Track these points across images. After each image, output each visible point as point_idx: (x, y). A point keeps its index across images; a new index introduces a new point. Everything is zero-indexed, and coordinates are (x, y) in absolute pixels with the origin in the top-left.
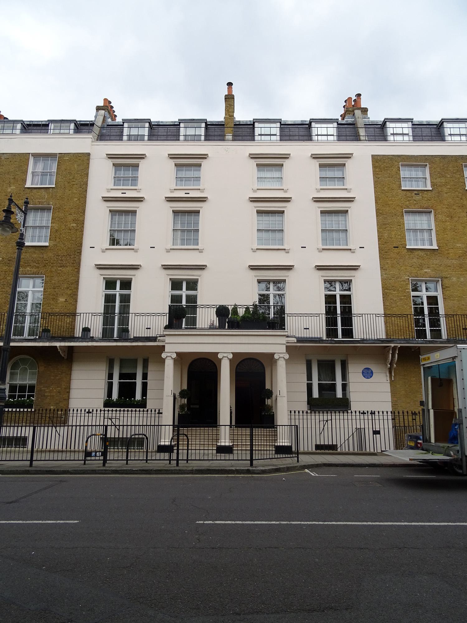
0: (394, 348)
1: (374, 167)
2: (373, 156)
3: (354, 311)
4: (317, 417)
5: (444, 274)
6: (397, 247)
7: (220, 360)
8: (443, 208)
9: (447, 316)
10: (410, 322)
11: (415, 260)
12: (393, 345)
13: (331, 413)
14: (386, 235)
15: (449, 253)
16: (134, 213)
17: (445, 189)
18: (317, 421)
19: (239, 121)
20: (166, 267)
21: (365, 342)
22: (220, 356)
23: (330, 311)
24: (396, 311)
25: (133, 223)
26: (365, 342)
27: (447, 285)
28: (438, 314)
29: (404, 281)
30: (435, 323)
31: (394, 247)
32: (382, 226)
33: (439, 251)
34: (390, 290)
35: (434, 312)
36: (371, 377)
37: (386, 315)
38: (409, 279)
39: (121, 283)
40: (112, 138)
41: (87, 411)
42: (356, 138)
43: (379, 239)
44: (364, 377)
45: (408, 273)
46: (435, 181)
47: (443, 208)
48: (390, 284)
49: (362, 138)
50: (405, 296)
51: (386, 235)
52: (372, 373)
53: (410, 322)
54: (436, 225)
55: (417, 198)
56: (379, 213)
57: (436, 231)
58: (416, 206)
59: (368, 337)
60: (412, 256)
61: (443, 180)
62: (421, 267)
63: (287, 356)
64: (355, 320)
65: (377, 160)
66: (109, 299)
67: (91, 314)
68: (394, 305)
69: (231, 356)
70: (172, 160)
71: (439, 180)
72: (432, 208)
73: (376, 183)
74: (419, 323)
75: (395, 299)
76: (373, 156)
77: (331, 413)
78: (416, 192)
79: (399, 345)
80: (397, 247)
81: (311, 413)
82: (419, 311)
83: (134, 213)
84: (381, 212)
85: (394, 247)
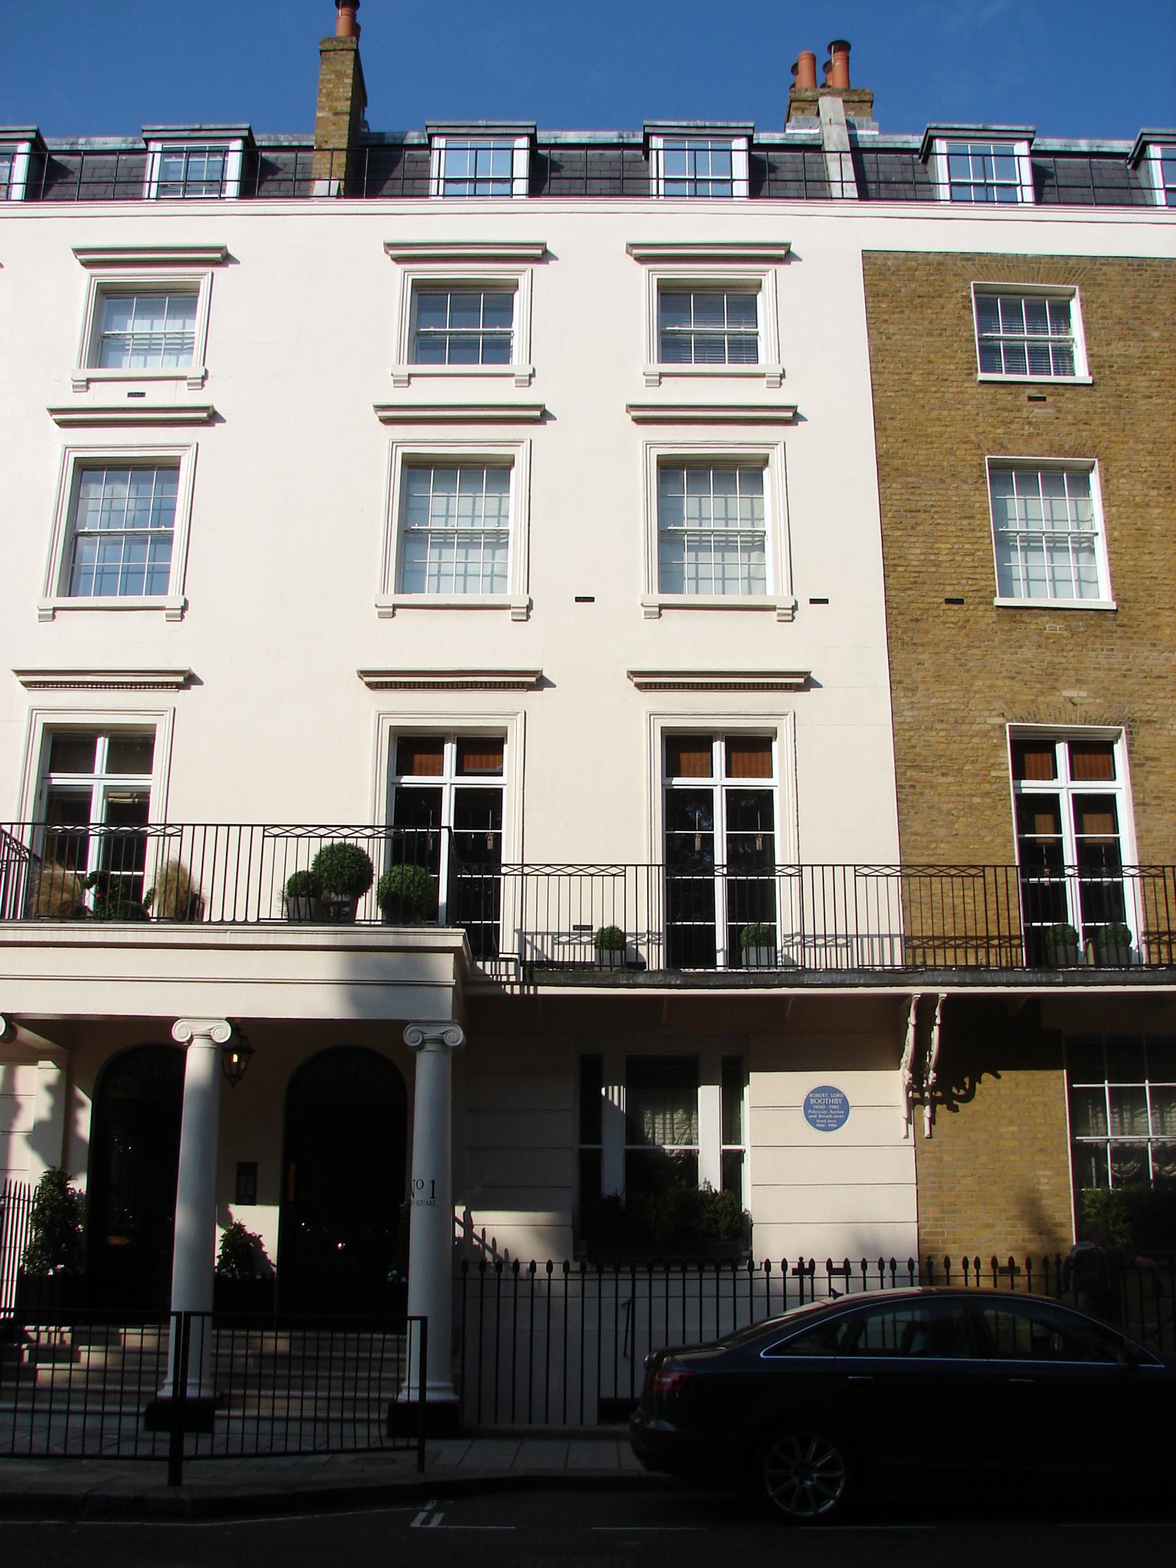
0: (926, 1002)
1: (873, 294)
2: (868, 256)
3: (782, 854)
4: (693, 1287)
5: (1141, 708)
6: (960, 602)
7: (410, 1055)
8: (1137, 452)
9: (1145, 871)
10: (1002, 899)
11: (1028, 653)
12: (917, 991)
13: (633, 1272)
14: (915, 553)
15: (1157, 627)
16: (168, 468)
17: (1141, 383)
18: (608, 1303)
19: (381, 135)
20: (650, 681)
21: (806, 979)
22: (411, 1037)
23: (683, 855)
24: (947, 852)
25: (165, 512)
26: (806, 979)
27: (1149, 752)
28: (1115, 867)
29: (985, 734)
30: (1103, 903)
31: (949, 601)
32: (900, 520)
33: (1122, 619)
34: (930, 770)
35: (1100, 857)
36: (840, 1122)
37: (908, 871)
38: (1002, 727)
39: (111, 745)
40: (596, 185)
41: (793, 1265)
42: (814, 188)
43: (889, 569)
44: (813, 1122)
45: (998, 705)
46: (1103, 351)
47: (1137, 452)
48: (927, 745)
49: (836, 190)
50: (987, 794)
51: (915, 553)
52: (845, 1106)
53: (1002, 899)
54: (1108, 520)
55: (1039, 412)
56: (888, 468)
57: (1111, 541)
58: (1035, 443)
59: (887, 962)
60: (1015, 635)
61: (1134, 349)
62: (1051, 678)
63: (456, 1036)
64: (785, 891)
65: (885, 275)
66: (684, 811)
67: (850, 871)
68: (941, 832)
69: (223, 1034)
70: (644, 268)
71: (1118, 348)
72: (1094, 451)
73: (878, 355)
74: (1047, 902)
75: (946, 807)
76: (868, 256)
77: (633, 1272)
78: (1033, 392)
79: (943, 991)
80: (960, 602)
81: (583, 1270)
82: (1040, 857)
83: (168, 468)
84: (897, 463)
85: (949, 601)
